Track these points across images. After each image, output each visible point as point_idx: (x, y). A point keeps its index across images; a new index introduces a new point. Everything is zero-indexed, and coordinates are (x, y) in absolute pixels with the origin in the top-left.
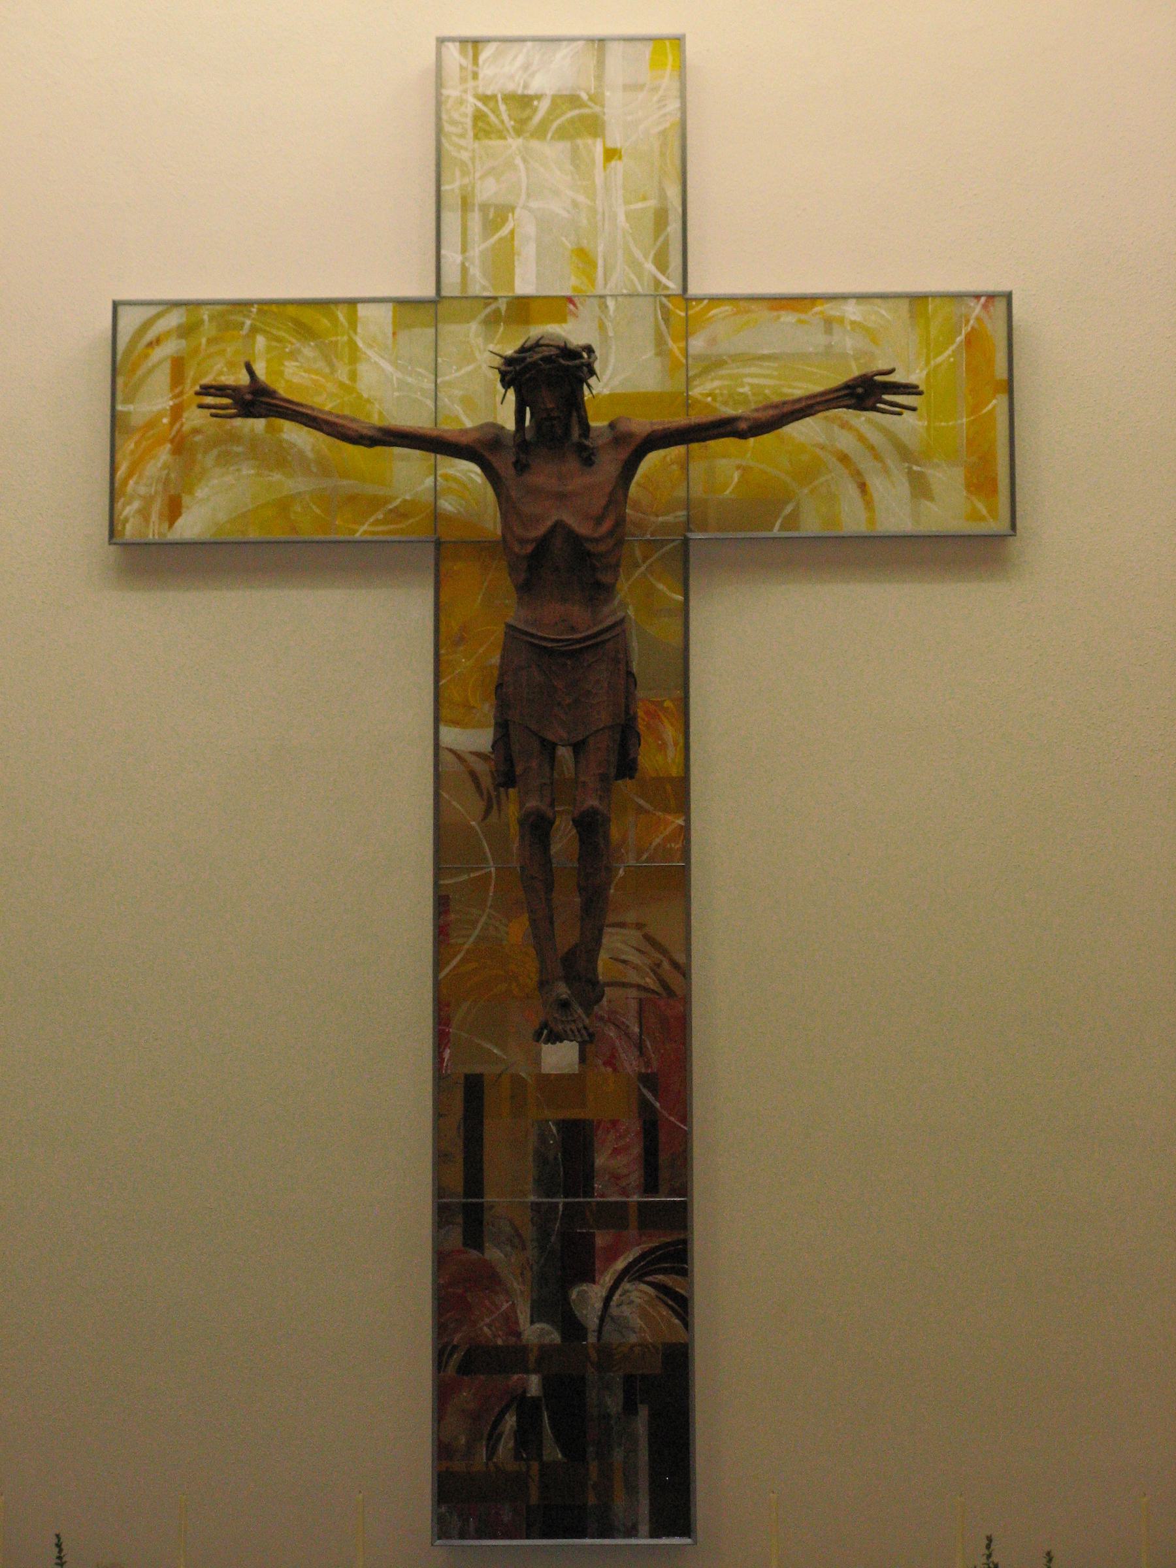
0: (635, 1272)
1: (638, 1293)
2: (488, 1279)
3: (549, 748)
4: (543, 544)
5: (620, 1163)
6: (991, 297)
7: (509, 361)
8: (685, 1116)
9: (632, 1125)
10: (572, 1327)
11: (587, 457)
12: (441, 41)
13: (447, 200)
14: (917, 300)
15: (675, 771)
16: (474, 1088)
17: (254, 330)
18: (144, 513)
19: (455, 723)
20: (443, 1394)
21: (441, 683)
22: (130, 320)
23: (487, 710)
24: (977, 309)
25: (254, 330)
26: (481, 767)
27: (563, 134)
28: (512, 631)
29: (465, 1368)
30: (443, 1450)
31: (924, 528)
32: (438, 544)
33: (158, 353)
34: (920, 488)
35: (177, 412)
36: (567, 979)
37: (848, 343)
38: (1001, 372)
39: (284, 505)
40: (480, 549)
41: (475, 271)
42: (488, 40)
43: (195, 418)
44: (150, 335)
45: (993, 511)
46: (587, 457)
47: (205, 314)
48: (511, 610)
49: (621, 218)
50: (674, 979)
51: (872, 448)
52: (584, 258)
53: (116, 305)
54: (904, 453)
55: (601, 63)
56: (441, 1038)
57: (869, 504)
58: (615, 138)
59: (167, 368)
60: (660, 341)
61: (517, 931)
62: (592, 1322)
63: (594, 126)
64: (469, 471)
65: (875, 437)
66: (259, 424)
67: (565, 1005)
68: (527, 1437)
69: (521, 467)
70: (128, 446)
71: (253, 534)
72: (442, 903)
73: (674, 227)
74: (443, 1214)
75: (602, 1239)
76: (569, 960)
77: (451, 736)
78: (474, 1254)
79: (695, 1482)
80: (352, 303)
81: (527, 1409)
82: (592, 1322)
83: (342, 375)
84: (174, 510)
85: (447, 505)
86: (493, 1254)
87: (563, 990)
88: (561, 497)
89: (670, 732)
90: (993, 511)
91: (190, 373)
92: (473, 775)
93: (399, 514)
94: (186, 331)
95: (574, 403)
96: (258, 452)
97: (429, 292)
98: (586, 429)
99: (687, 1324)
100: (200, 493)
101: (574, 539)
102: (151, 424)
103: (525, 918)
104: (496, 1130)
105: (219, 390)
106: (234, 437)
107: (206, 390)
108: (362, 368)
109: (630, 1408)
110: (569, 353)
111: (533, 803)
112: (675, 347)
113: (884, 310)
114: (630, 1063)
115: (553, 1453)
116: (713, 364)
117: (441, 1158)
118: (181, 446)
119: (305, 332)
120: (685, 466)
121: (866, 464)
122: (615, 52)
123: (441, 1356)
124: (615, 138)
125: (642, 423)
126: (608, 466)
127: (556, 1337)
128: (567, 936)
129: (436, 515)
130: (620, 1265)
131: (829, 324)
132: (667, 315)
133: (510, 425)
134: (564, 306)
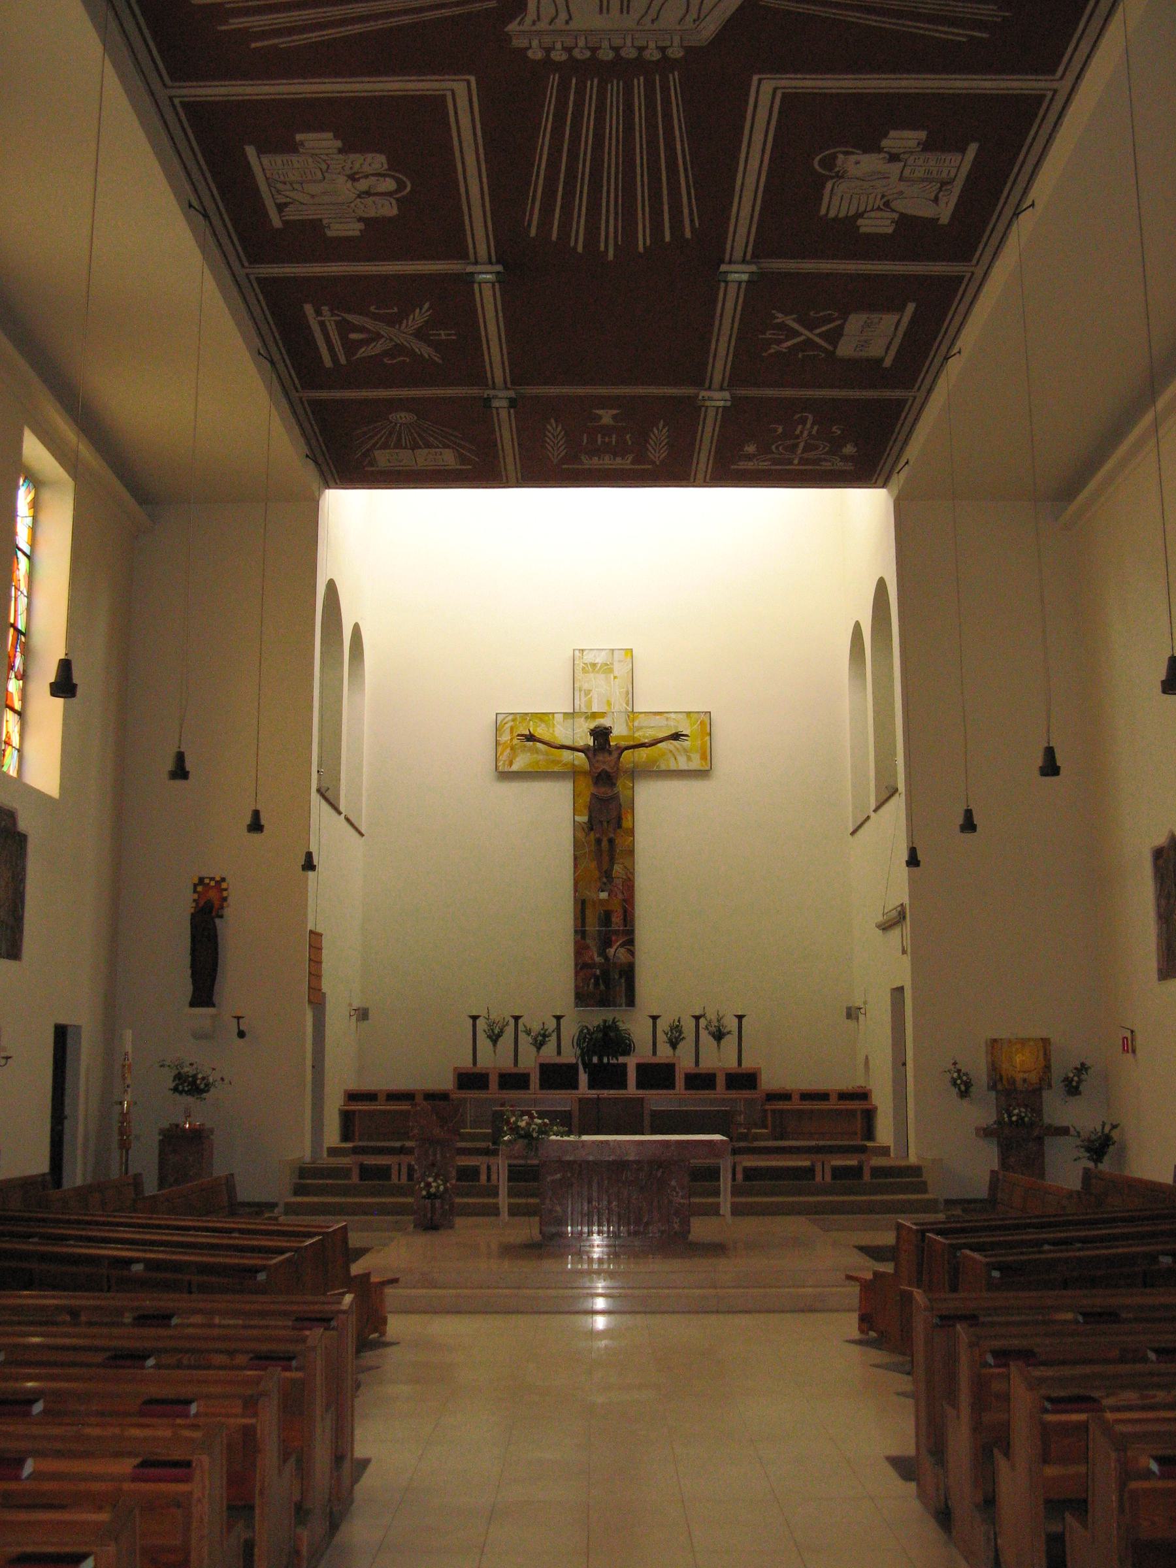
0: (622, 946)
1: (622, 950)
2: (587, 947)
3: (601, 822)
4: (600, 774)
5: (618, 920)
6: (706, 712)
7: (592, 730)
8: (633, 909)
9: (620, 911)
10: (607, 958)
11: (610, 753)
12: (574, 650)
13: (576, 689)
14: (688, 713)
15: (631, 827)
16: (583, 902)
17: (530, 720)
18: (504, 764)
19: (578, 815)
20: (577, 973)
21: (1067, 1515)
22: (500, 718)
23: (586, 811)
24: (702, 715)
25: (530, 720)
26: (585, 826)
27: (604, 672)
28: (593, 794)
29: (581, 969)
30: (577, 987)
31: (691, 768)
32: (574, 772)
33: (507, 725)
34: (689, 759)
35: (511, 739)
36: (606, 877)
37: (672, 723)
38: (709, 731)
39: (537, 763)
40: (584, 773)
41: (582, 706)
42: (585, 650)
43: (515, 741)
44: (505, 722)
45: (706, 764)
46: (610, 753)
47: (518, 716)
48: (593, 789)
49: (618, 693)
50: (630, 876)
51: (678, 749)
52: (609, 703)
53: (497, 714)
54: (685, 751)
55: (613, 654)
56: (576, 891)
57: (677, 763)
58: (616, 674)
59: (509, 730)
60: (627, 725)
61: (593, 865)
62: (612, 958)
63: (611, 671)
64: (582, 755)
65: (678, 746)
66: (531, 743)
67: (605, 884)
68: (597, 984)
69: (595, 755)
70: (500, 749)
71: (530, 770)
72: (575, 858)
73: (630, 695)
74: (576, 932)
75: (614, 938)
76: (606, 872)
77: (577, 818)
78: (583, 941)
79: (709, 1068)
80: (554, 713)
81: (597, 979)
82: (612, 958)
83: (551, 731)
84: (511, 764)
85: (576, 763)
86: (588, 941)
87: (605, 880)
88: (604, 762)
89: (630, 818)
90: (706, 764)
91: (515, 730)
92: (583, 828)
93: (565, 765)
94: (513, 720)
95: (607, 741)
96: (530, 750)
97: (572, 711)
98: (610, 745)
99: (634, 957)
100: (517, 759)
101: (606, 772)
102: (506, 742)
103: (596, 862)
104: (588, 912)
105: (522, 735)
106: (525, 746)
107: (518, 735)
108: (556, 729)
109: (621, 977)
110: (606, 729)
111: (598, 835)
112: (630, 724)
113: (680, 716)
114: (620, 896)
115: (602, 987)
116: (640, 728)
117: (576, 919)
118: (512, 748)
119: (542, 720)
120: (633, 753)
121: (676, 753)
122: (615, 652)
123: (576, 965)
124: (616, 674)
125: (623, 744)
126: (615, 755)
127: (603, 961)
128: (605, 867)
129: (574, 765)
130: (618, 943)
131: (667, 719)
132: (629, 716)
133: (592, 744)
134: (603, 715)
